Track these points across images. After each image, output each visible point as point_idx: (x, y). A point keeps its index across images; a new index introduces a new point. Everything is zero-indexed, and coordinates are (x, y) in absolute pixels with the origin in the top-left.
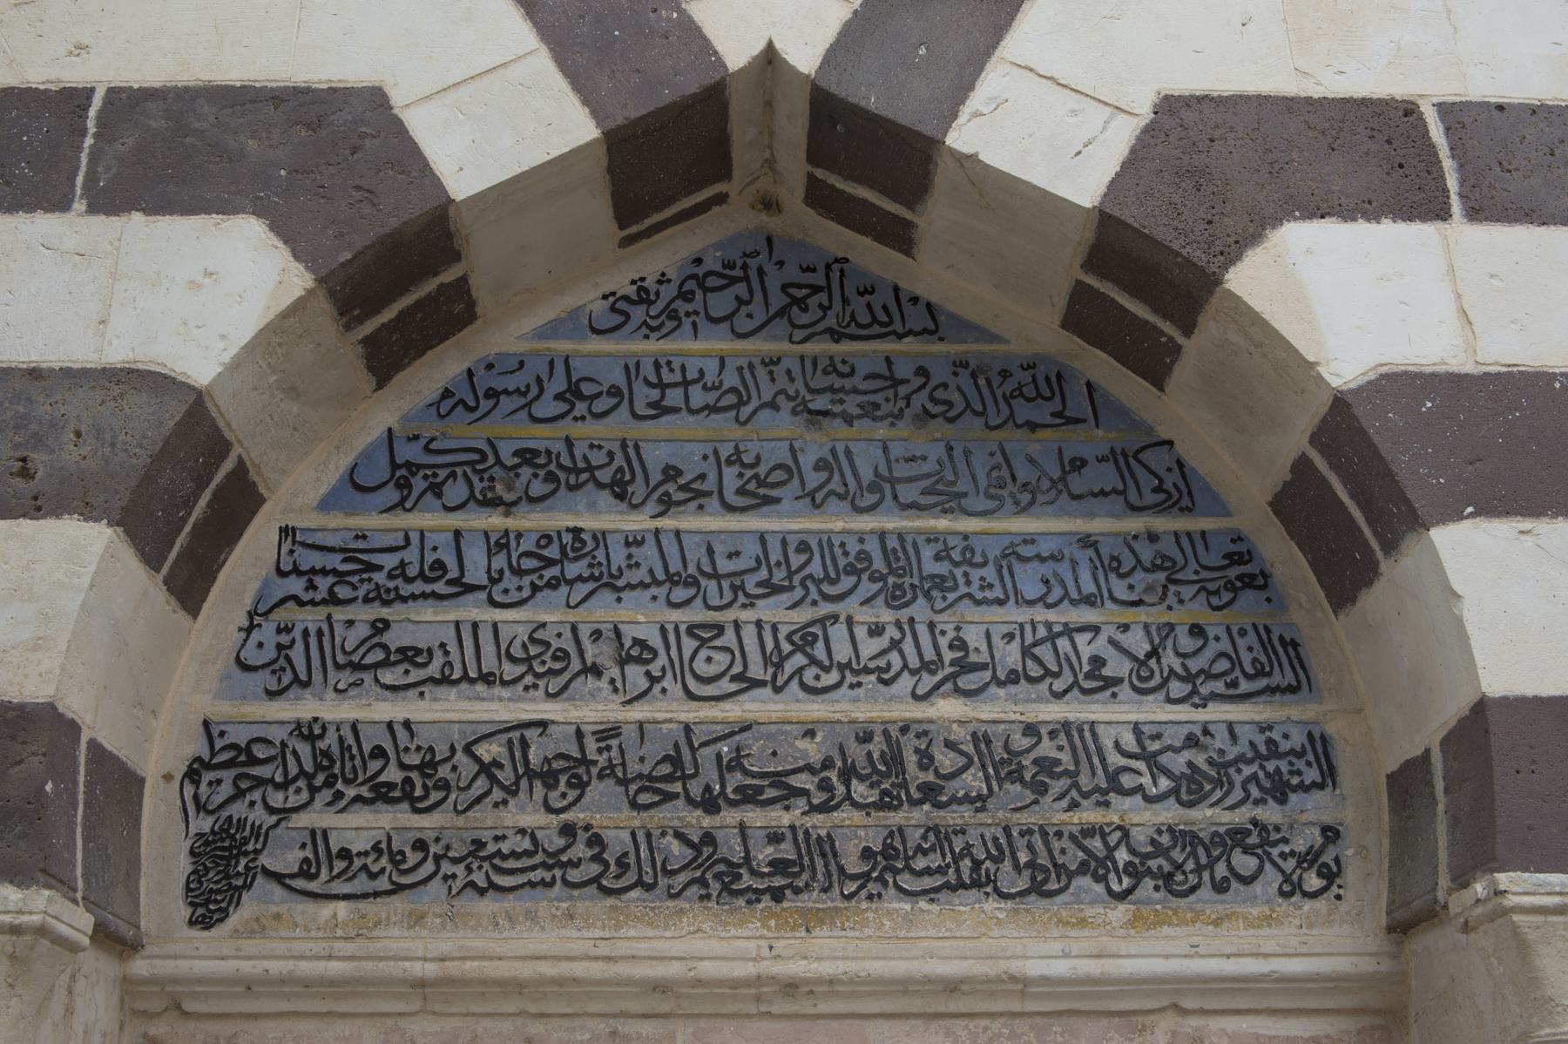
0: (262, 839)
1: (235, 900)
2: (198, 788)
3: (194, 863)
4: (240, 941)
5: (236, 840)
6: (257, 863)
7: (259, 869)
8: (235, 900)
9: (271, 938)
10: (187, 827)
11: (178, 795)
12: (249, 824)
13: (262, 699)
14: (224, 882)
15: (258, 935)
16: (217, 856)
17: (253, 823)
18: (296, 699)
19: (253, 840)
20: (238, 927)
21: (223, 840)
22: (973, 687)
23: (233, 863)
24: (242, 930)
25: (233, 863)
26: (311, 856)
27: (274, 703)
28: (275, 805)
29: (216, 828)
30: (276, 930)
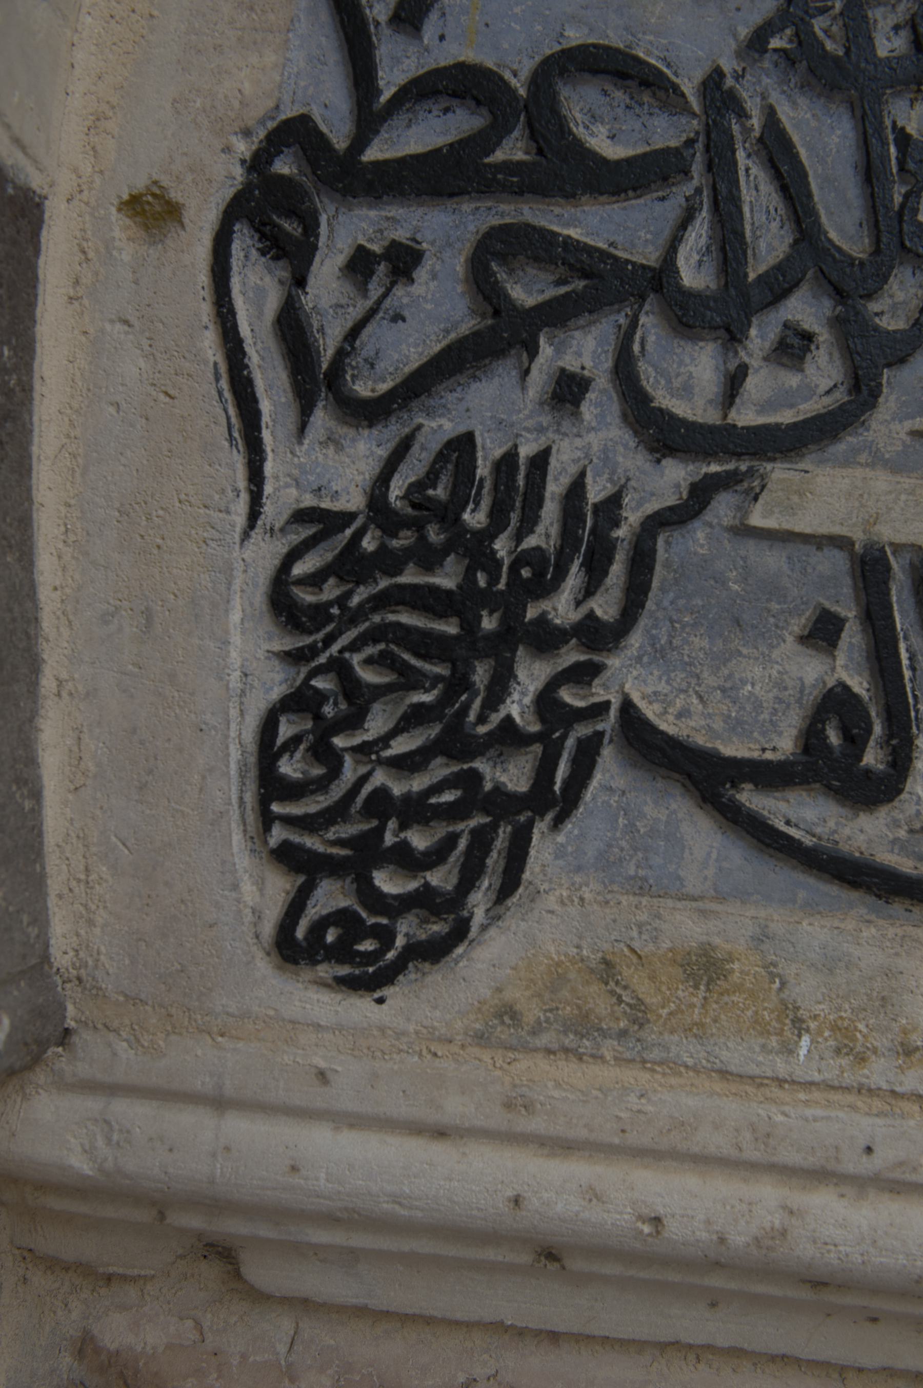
0: (617, 570)
1: (495, 860)
2: (300, 281)
3: (294, 657)
4: (524, 1063)
5: (492, 565)
6: (599, 693)
7: (609, 723)
8: (495, 860)
9: (672, 1066)
10: (256, 476)
11: (206, 310)
12: (555, 488)
14: (440, 769)
15: (608, 1048)
16: (404, 635)
17: (577, 488)
19: (574, 579)
20: (513, 994)
21: (430, 562)
23: (481, 674)
24: (532, 1012)
25: (481, 674)
26: (859, 685)
29: (396, 490)
30: (697, 1031)
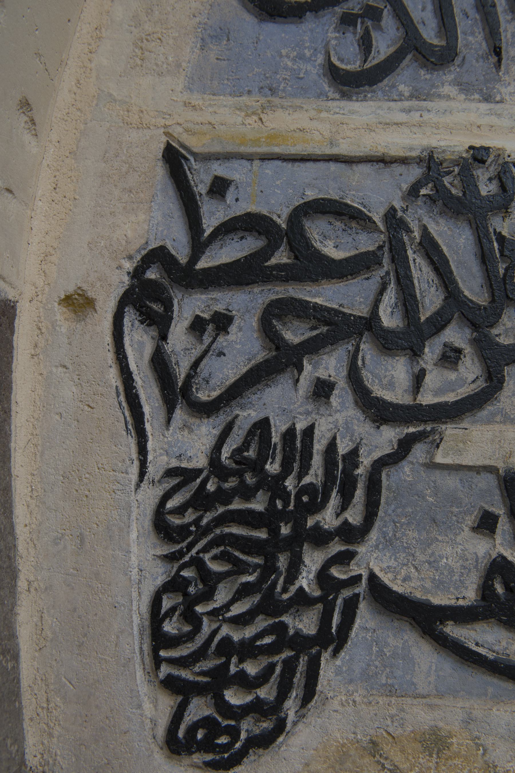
0: (359, 494)
2: (164, 337)
3: (170, 558)
5: (285, 496)
7: (362, 588)
11: (110, 357)
13: (321, 95)
17: (332, 447)
18: (415, 95)
19: (334, 500)
22: (451, 398)
27: (355, 106)
28: (388, 396)
29: (225, 453)
